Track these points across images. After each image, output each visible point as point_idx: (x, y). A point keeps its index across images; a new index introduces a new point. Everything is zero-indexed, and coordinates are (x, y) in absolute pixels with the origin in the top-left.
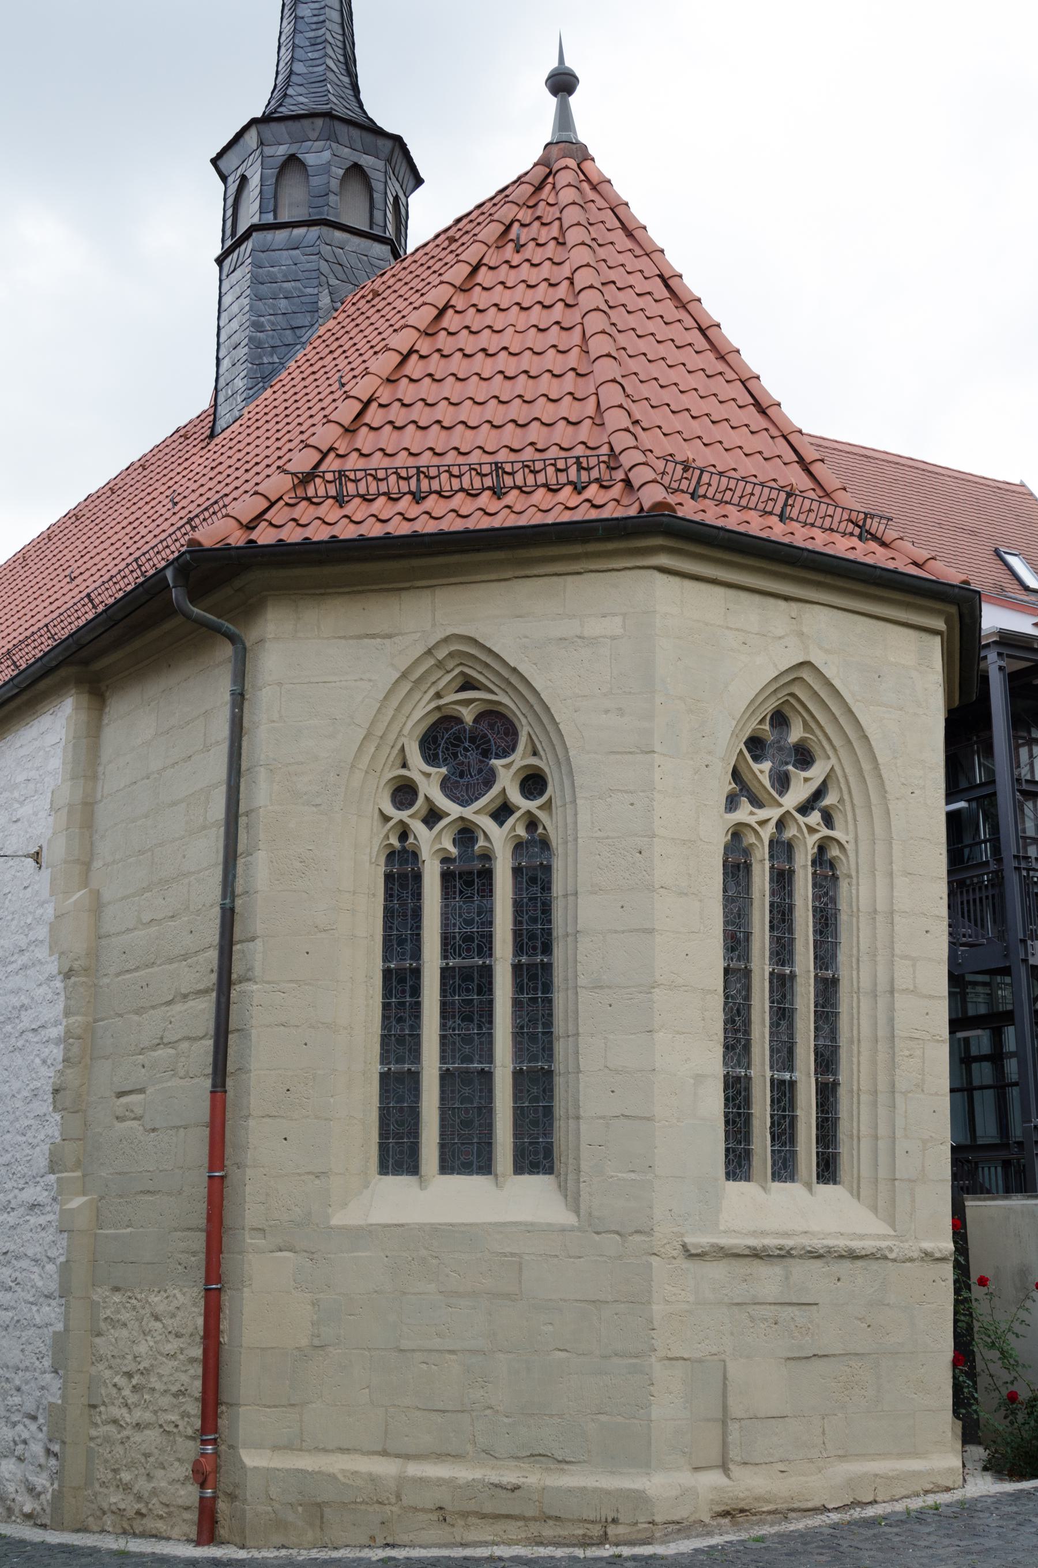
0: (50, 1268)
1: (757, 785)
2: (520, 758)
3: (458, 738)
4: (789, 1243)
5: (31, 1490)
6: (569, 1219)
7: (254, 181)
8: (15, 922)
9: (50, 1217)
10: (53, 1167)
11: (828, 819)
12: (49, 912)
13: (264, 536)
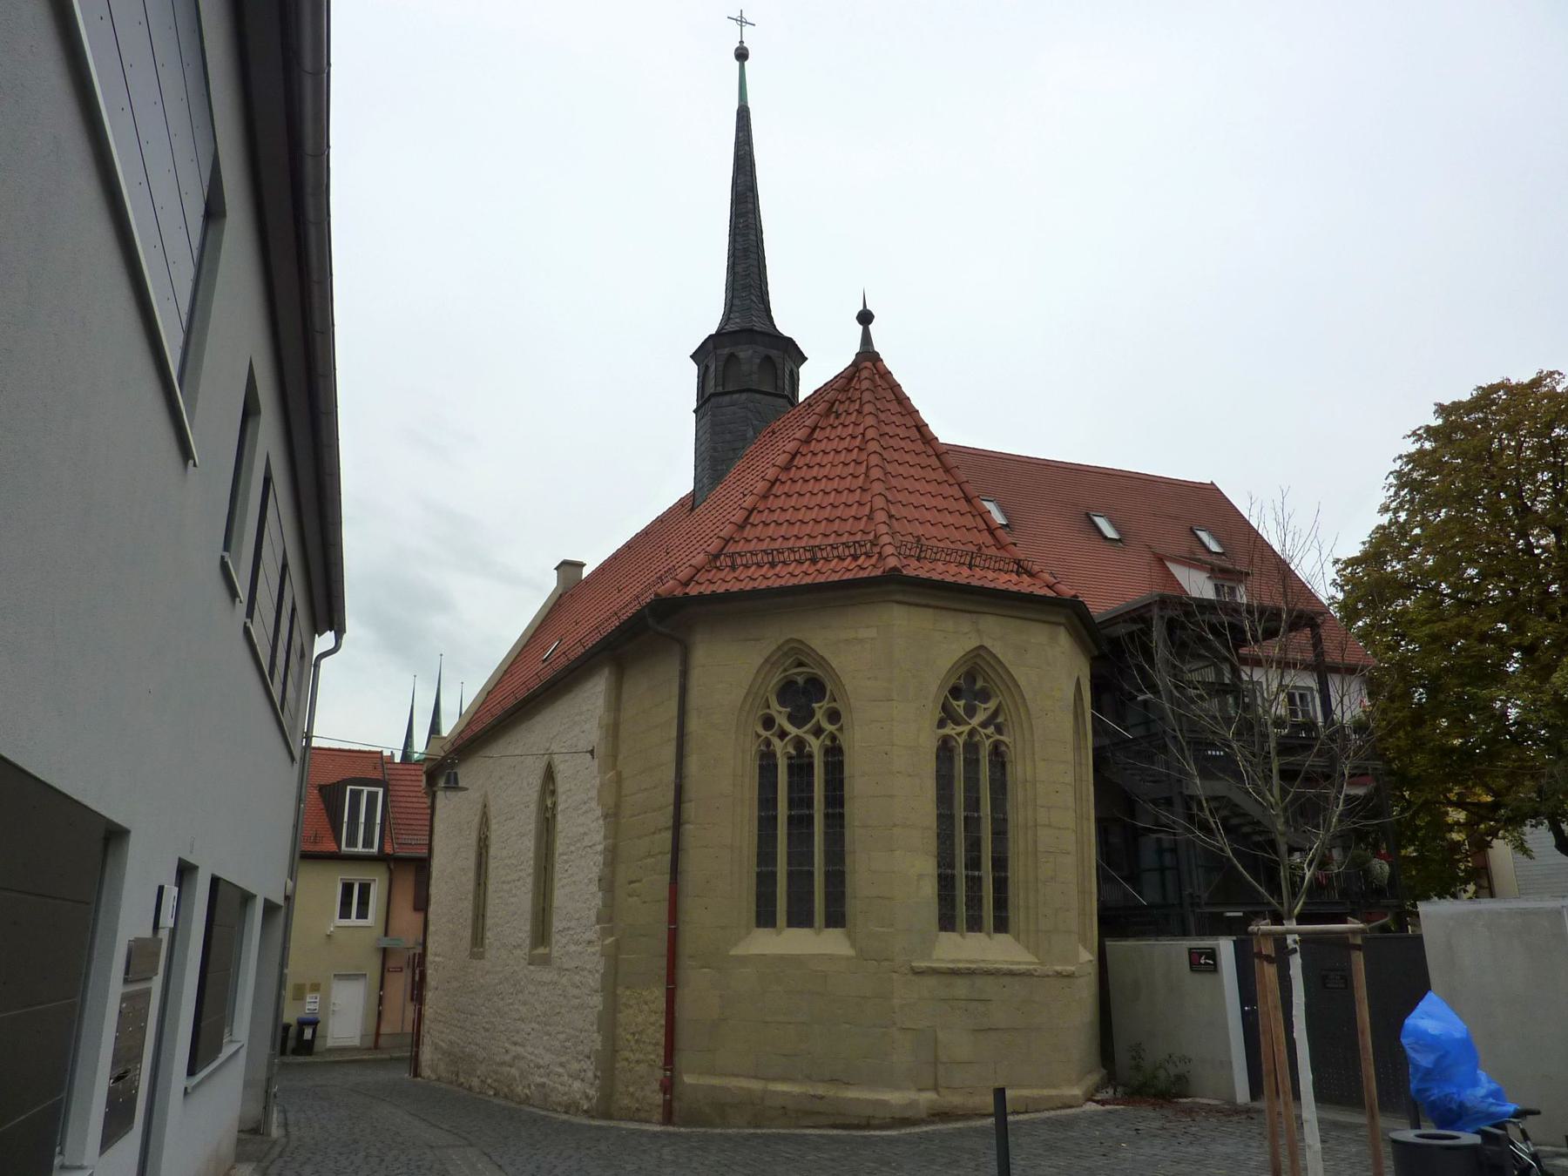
4: (973, 966)
6: (851, 952)
7: (712, 369)
11: (999, 730)
12: (597, 782)
13: (693, 590)
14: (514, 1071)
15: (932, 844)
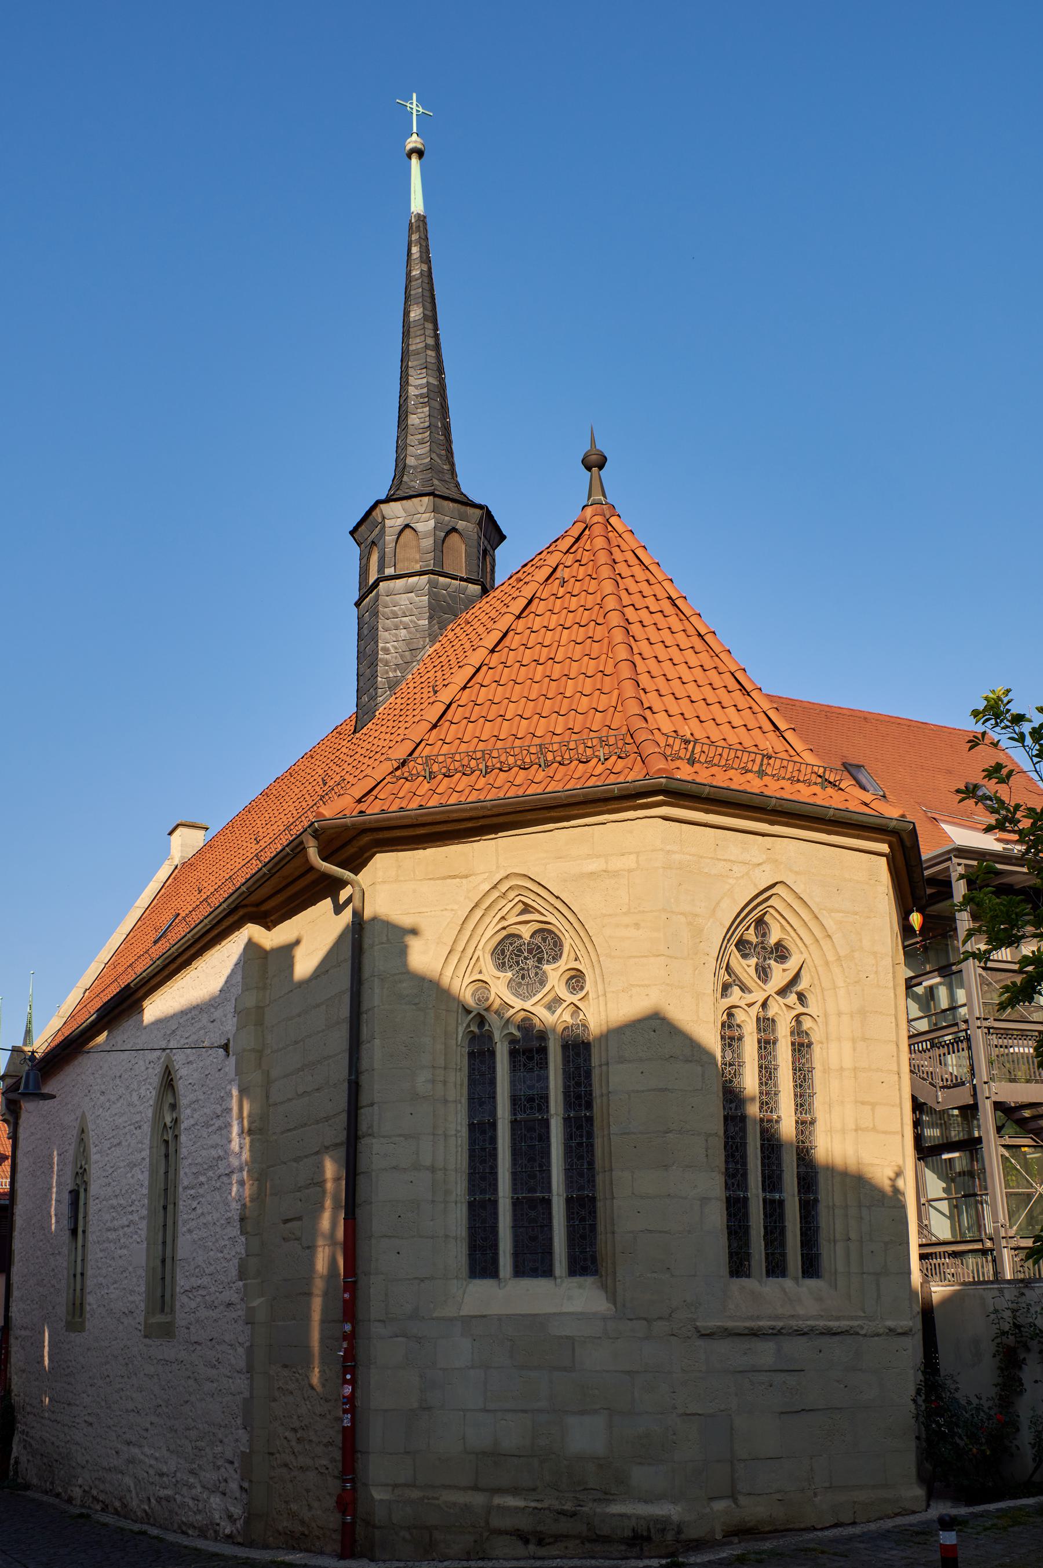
0: (241, 1350)
1: (746, 976)
2: (565, 962)
3: (520, 951)
5: (230, 1517)
8: (213, 1096)
9: (240, 1313)
10: (242, 1275)
11: (801, 997)
14: (128, 1481)
15: (719, 1158)
